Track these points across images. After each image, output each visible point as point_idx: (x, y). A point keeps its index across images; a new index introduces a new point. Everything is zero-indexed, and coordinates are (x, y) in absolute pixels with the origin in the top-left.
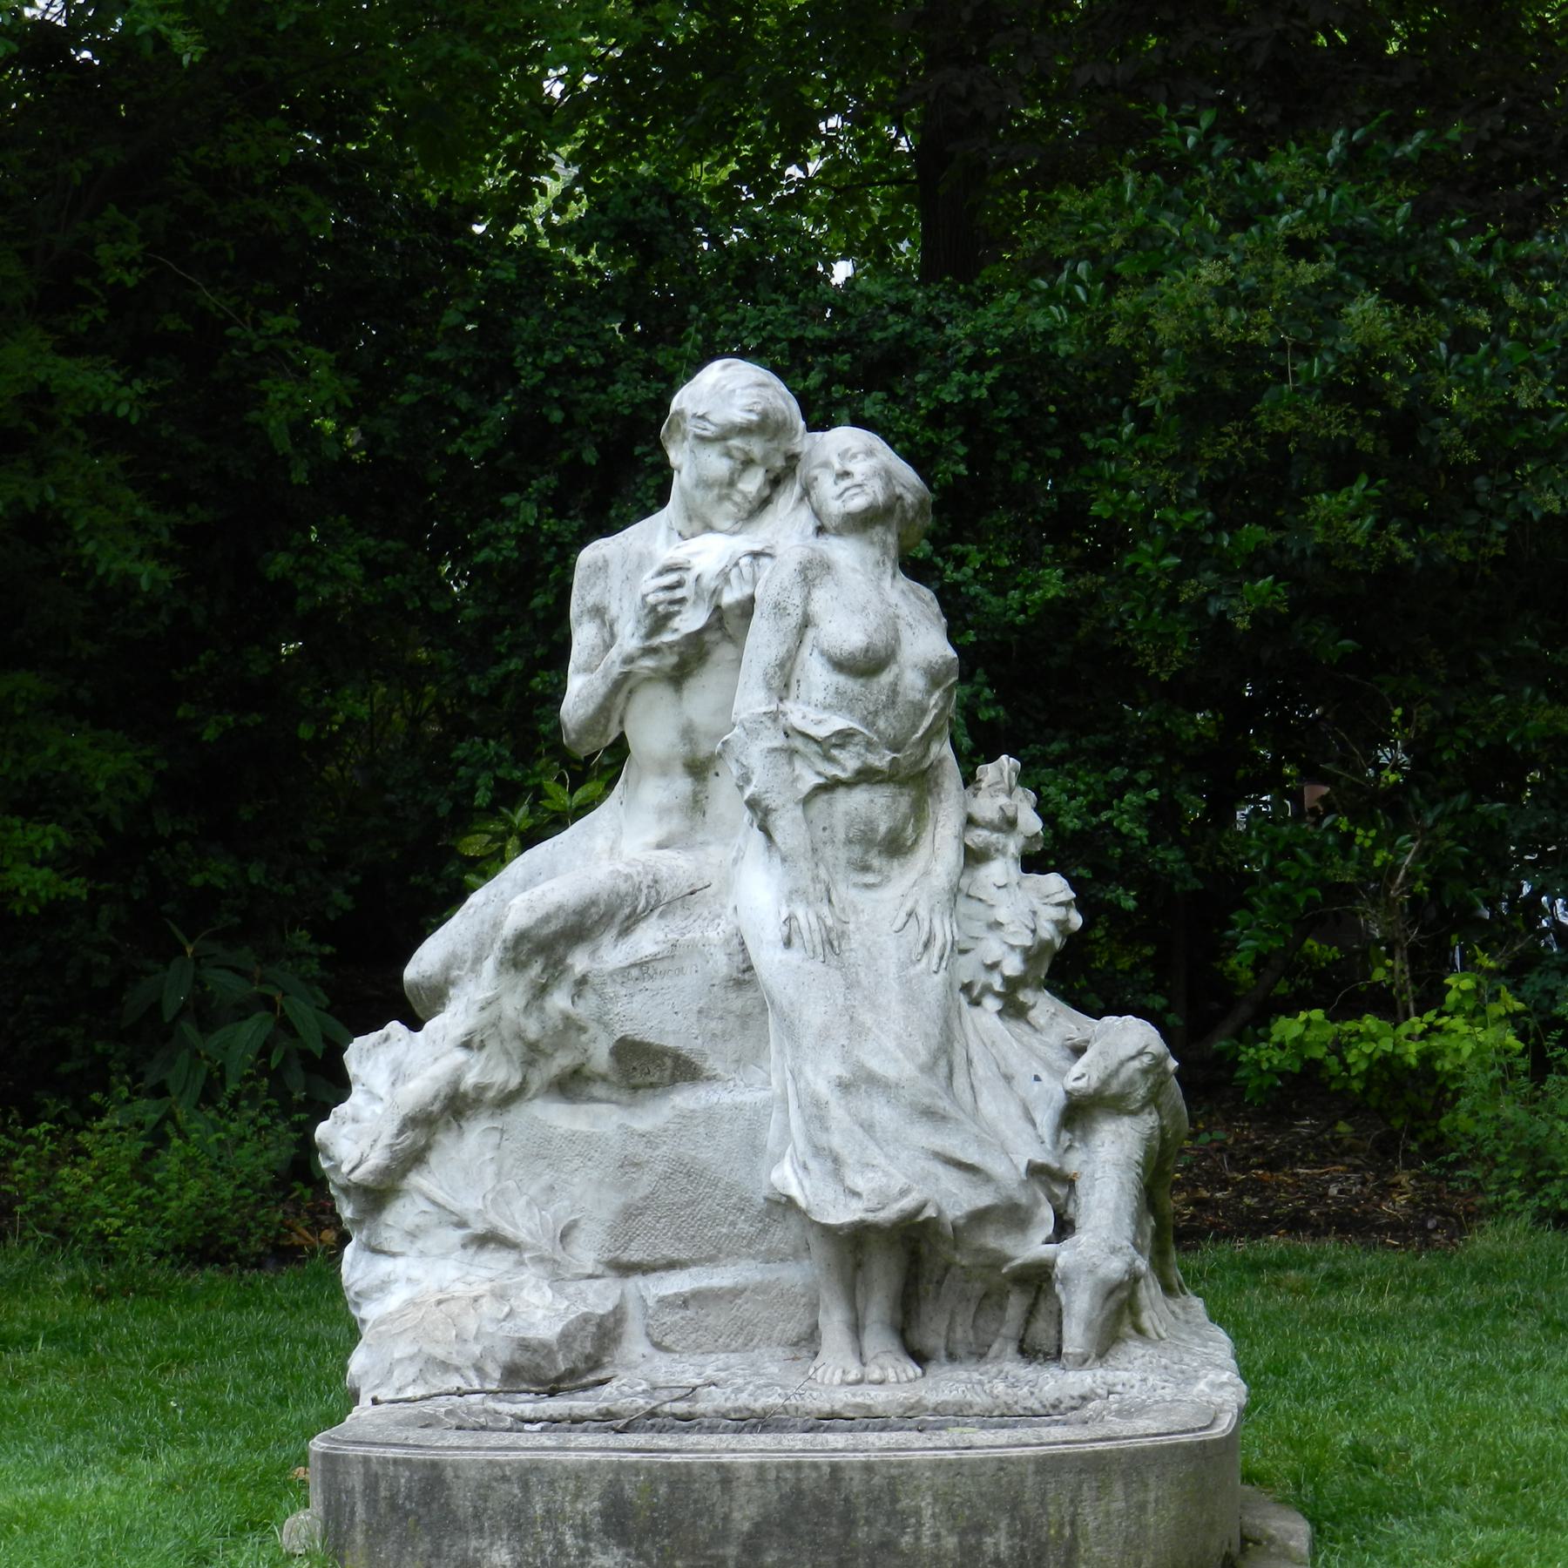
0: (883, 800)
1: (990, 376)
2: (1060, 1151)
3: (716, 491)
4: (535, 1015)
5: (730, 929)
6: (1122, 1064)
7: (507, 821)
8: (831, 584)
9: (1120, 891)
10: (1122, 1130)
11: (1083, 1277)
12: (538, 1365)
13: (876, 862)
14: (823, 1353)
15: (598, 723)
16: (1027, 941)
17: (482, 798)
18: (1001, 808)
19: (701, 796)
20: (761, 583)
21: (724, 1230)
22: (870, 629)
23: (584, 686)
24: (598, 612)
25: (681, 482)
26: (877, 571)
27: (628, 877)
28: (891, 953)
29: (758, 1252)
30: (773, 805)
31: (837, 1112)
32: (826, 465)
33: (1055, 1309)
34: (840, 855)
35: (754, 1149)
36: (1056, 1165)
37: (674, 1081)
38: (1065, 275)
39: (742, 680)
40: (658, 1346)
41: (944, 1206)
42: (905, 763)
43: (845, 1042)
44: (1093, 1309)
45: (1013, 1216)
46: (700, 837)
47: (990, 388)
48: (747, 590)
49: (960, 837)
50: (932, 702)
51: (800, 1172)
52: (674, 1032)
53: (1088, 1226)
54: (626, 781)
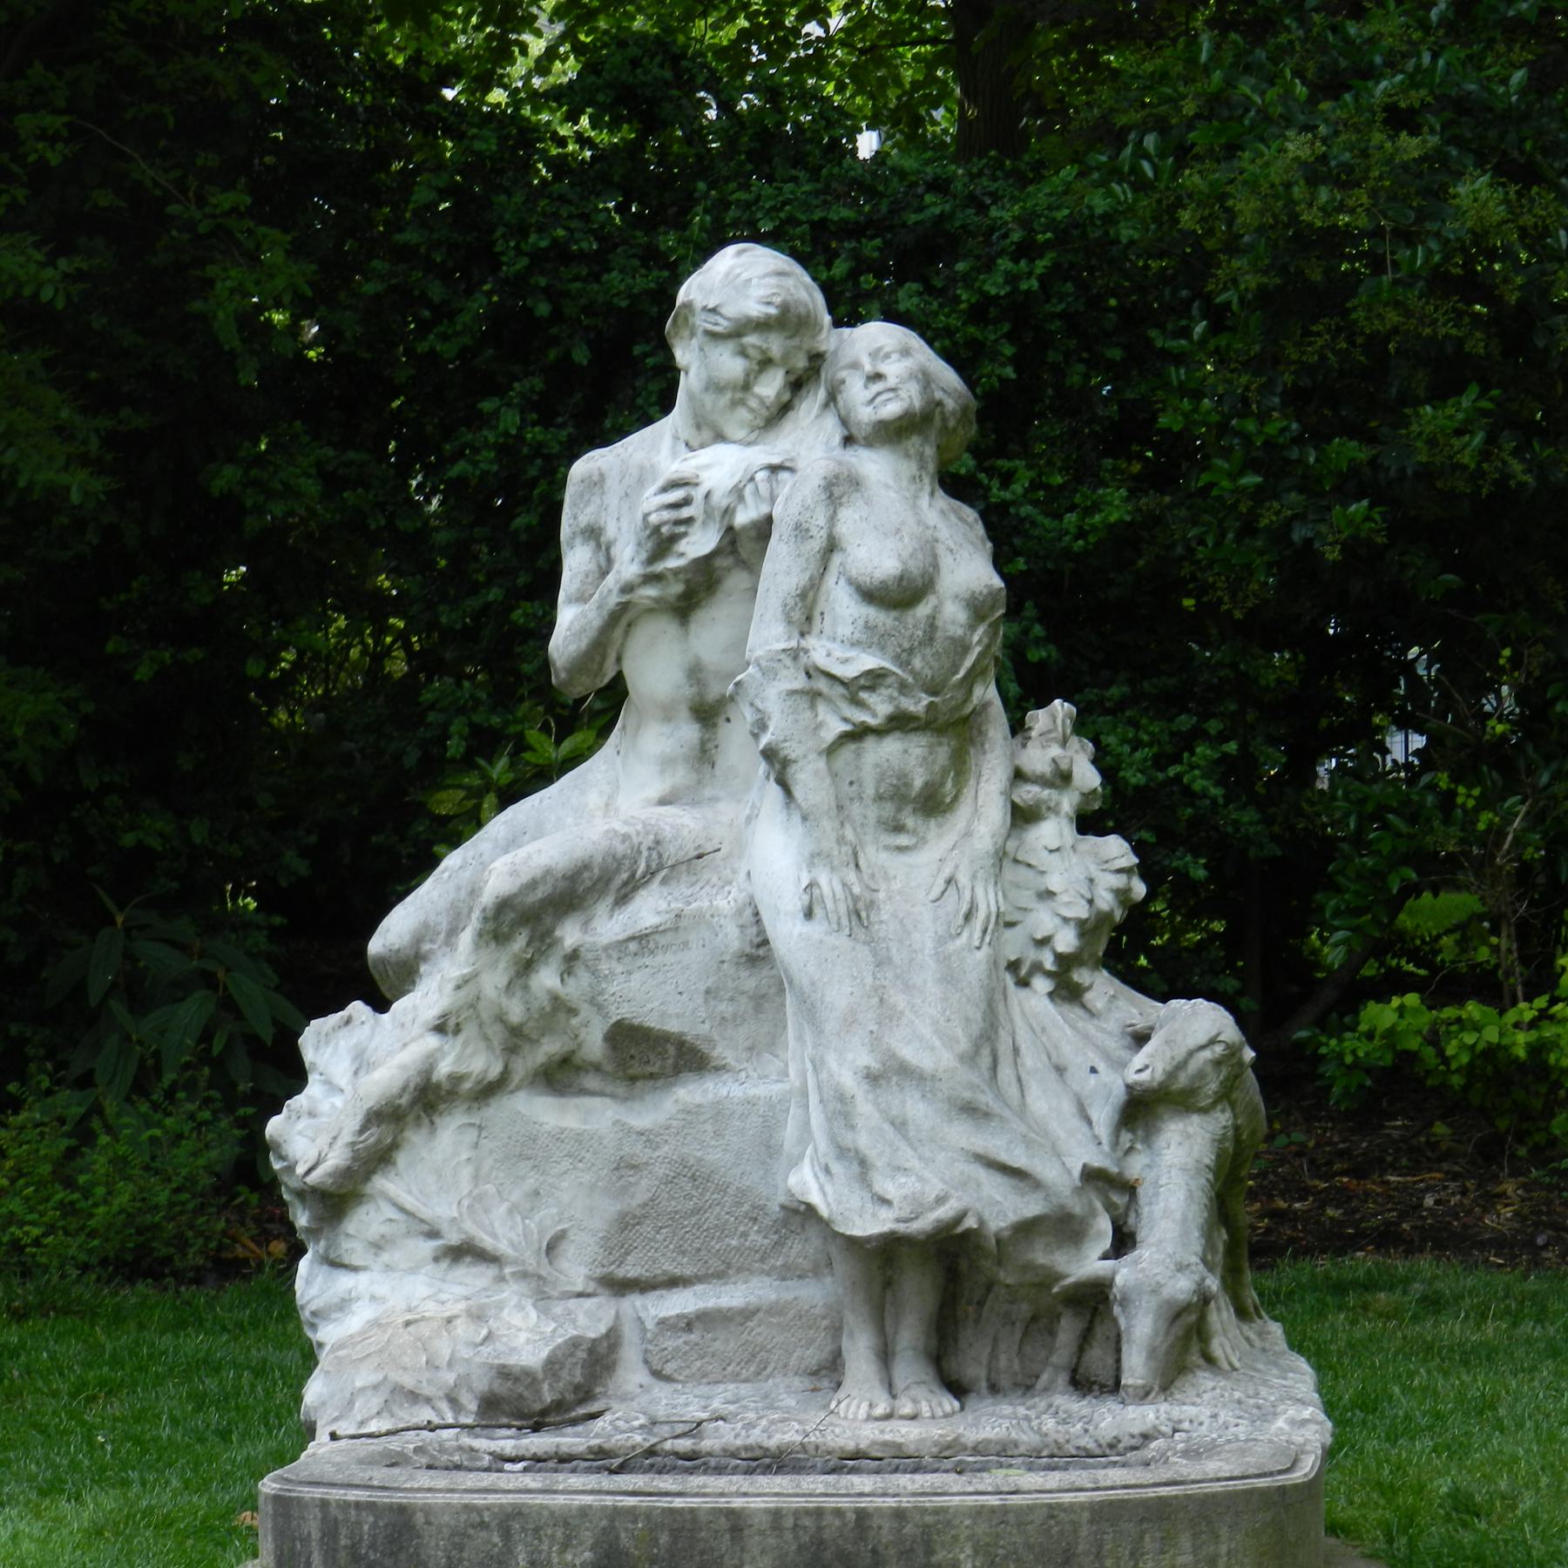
0: (918, 751)
1: (1041, 265)
2: (1120, 1154)
3: (729, 395)
6: (1191, 1054)
7: (485, 776)
8: (860, 503)
9: (1188, 858)
10: (1191, 1130)
11: (1145, 1298)
12: (521, 1396)
13: (910, 821)
16: (1082, 912)
17: (455, 747)
18: (1054, 760)
21: (734, 1243)
22: (905, 554)
23: (576, 618)
24: (593, 533)
25: (688, 384)
26: (913, 488)
27: (626, 838)
28: (927, 927)
29: (773, 1268)
30: (793, 756)
31: (865, 1107)
32: (855, 366)
33: (1112, 1335)
35: (769, 1150)
36: (1114, 1170)
40: (658, 1374)
41: (986, 1216)
43: (874, 1028)
44: (1156, 1334)
45: (1064, 1228)
46: (708, 792)
47: (1041, 278)
48: (764, 509)
49: (1007, 794)
50: (976, 638)
52: (678, 1016)
53: (1152, 1240)
54: (624, 727)
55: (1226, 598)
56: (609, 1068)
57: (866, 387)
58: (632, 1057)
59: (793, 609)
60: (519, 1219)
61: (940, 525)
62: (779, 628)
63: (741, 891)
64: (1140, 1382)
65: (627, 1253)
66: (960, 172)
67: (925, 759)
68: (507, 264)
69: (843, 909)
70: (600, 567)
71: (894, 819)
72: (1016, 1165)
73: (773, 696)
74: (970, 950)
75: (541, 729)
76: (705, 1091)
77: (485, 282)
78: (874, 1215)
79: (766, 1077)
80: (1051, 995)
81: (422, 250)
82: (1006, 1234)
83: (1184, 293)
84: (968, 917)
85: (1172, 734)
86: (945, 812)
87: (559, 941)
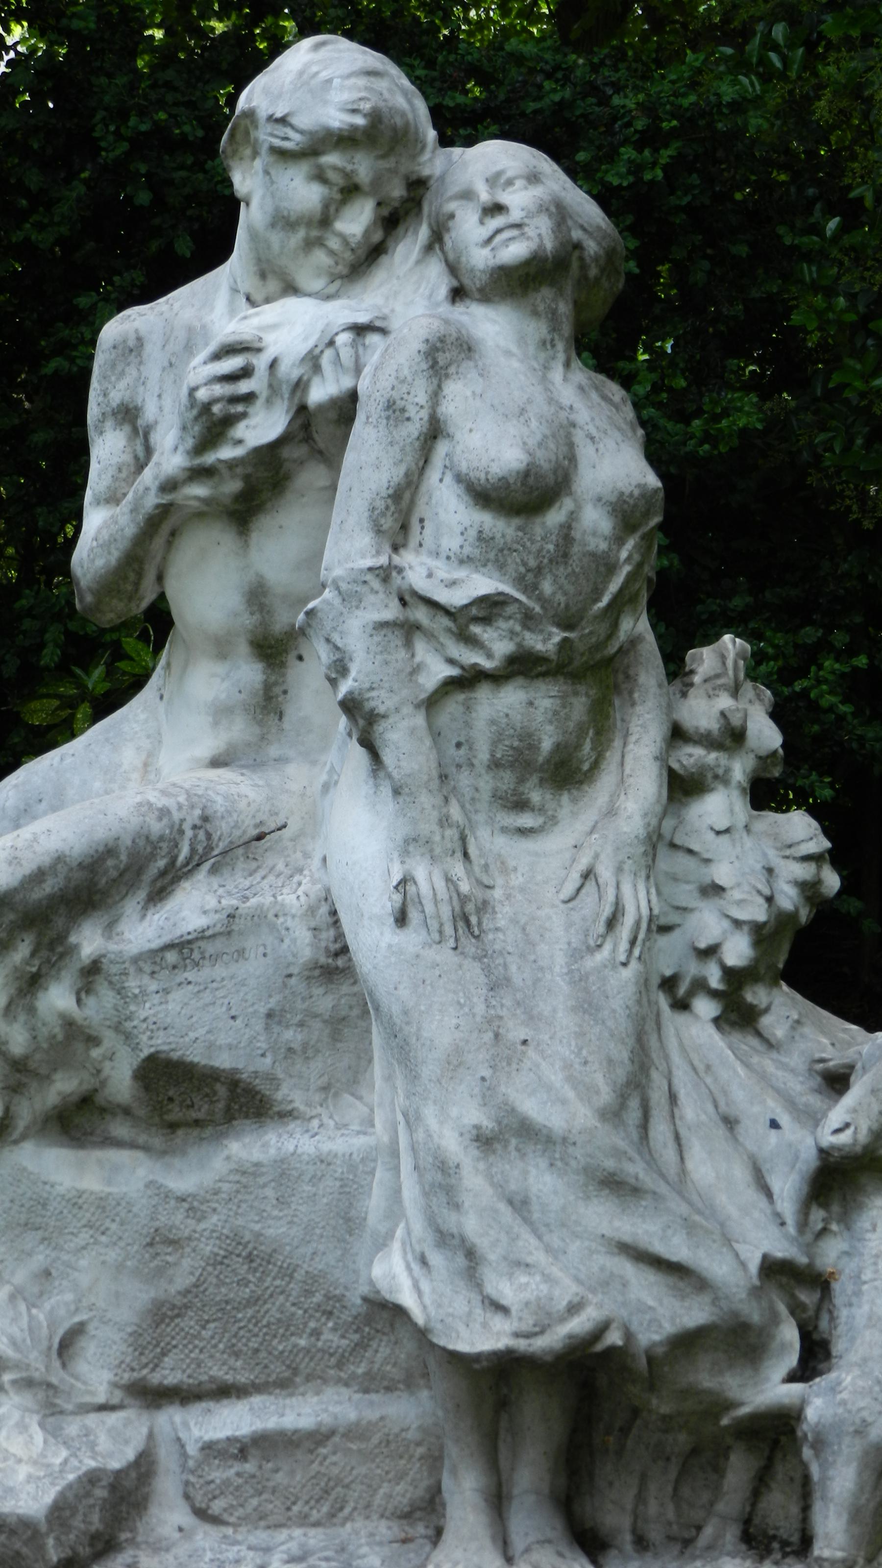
0: (547, 703)
1: (666, 155)
2: (809, 1237)
3: (301, 233)
4: (22, 1018)
5: (316, 890)
7: (81, 686)
8: (473, 374)
9: (814, 776)
11: (847, 1440)
12: (18, 1553)
13: (536, 797)
14: (448, 1537)
15: (125, 578)
16: (758, 913)
17: (50, 656)
18: (723, 714)
19: (277, 690)
20: (367, 371)
21: (302, 1342)
22: (532, 442)
23: (105, 525)
24: (127, 414)
25: (251, 218)
26: (543, 355)
27: (164, 812)
28: (557, 933)
29: (353, 1376)
30: (382, 709)
31: (474, 1180)
32: (467, 195)
33: (798, 1476)
34: (482, 784)
35: (349, 1223)
36: (803, 1260)
37: (229, 1117)
38: (757, 40)
39: (336, 519)
40: (202, 1514)
41: (634, 1327)
42: (581, 647)
43: (487, 1073)
44: (861, 1488)
45: (740, 1341)
46: (274, 751)
47: (665, 168)
48: (347, 383)
49: (662, 759)
50: (624, 554)
51: (416, 1267)
52: (230, 1047)
53: (853, 1357)
54: (168, 665)
55: (855, 508)
56: (141, 1112)
57: (482, 222)
58: (171, 1099)
59: (383, 514)
60: (23, 1307)
61: (578, 405)
62: (365, 540)
63: (314, 882)
64: (839, 1554)
65: (164, 1354)
66: (581, 61)
67: (556, 713)
68: (105, 150)
69: (446, 912)
70: (136, 458)
71: (515, 792)
72: (674, 1258)
73: (357, 630)
74: (614, 967)
75: (139, 638)
76: (265, 1145)
77: (83, 170)
78: (485, 1325)
79: (346, 1126)
80: (717, 1021)
81: (19, 136)
82: (660, 1350)
83: (811, 191)
84: (612, 923)
85: (796, 646)
86: (581, 782)
87: (74, 949)
